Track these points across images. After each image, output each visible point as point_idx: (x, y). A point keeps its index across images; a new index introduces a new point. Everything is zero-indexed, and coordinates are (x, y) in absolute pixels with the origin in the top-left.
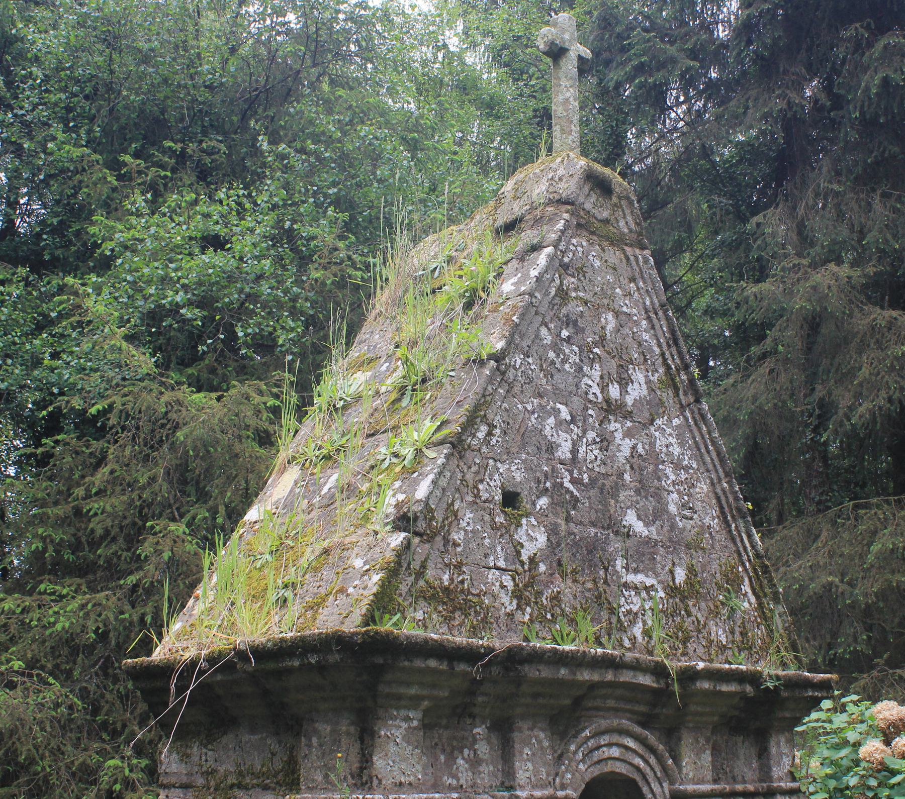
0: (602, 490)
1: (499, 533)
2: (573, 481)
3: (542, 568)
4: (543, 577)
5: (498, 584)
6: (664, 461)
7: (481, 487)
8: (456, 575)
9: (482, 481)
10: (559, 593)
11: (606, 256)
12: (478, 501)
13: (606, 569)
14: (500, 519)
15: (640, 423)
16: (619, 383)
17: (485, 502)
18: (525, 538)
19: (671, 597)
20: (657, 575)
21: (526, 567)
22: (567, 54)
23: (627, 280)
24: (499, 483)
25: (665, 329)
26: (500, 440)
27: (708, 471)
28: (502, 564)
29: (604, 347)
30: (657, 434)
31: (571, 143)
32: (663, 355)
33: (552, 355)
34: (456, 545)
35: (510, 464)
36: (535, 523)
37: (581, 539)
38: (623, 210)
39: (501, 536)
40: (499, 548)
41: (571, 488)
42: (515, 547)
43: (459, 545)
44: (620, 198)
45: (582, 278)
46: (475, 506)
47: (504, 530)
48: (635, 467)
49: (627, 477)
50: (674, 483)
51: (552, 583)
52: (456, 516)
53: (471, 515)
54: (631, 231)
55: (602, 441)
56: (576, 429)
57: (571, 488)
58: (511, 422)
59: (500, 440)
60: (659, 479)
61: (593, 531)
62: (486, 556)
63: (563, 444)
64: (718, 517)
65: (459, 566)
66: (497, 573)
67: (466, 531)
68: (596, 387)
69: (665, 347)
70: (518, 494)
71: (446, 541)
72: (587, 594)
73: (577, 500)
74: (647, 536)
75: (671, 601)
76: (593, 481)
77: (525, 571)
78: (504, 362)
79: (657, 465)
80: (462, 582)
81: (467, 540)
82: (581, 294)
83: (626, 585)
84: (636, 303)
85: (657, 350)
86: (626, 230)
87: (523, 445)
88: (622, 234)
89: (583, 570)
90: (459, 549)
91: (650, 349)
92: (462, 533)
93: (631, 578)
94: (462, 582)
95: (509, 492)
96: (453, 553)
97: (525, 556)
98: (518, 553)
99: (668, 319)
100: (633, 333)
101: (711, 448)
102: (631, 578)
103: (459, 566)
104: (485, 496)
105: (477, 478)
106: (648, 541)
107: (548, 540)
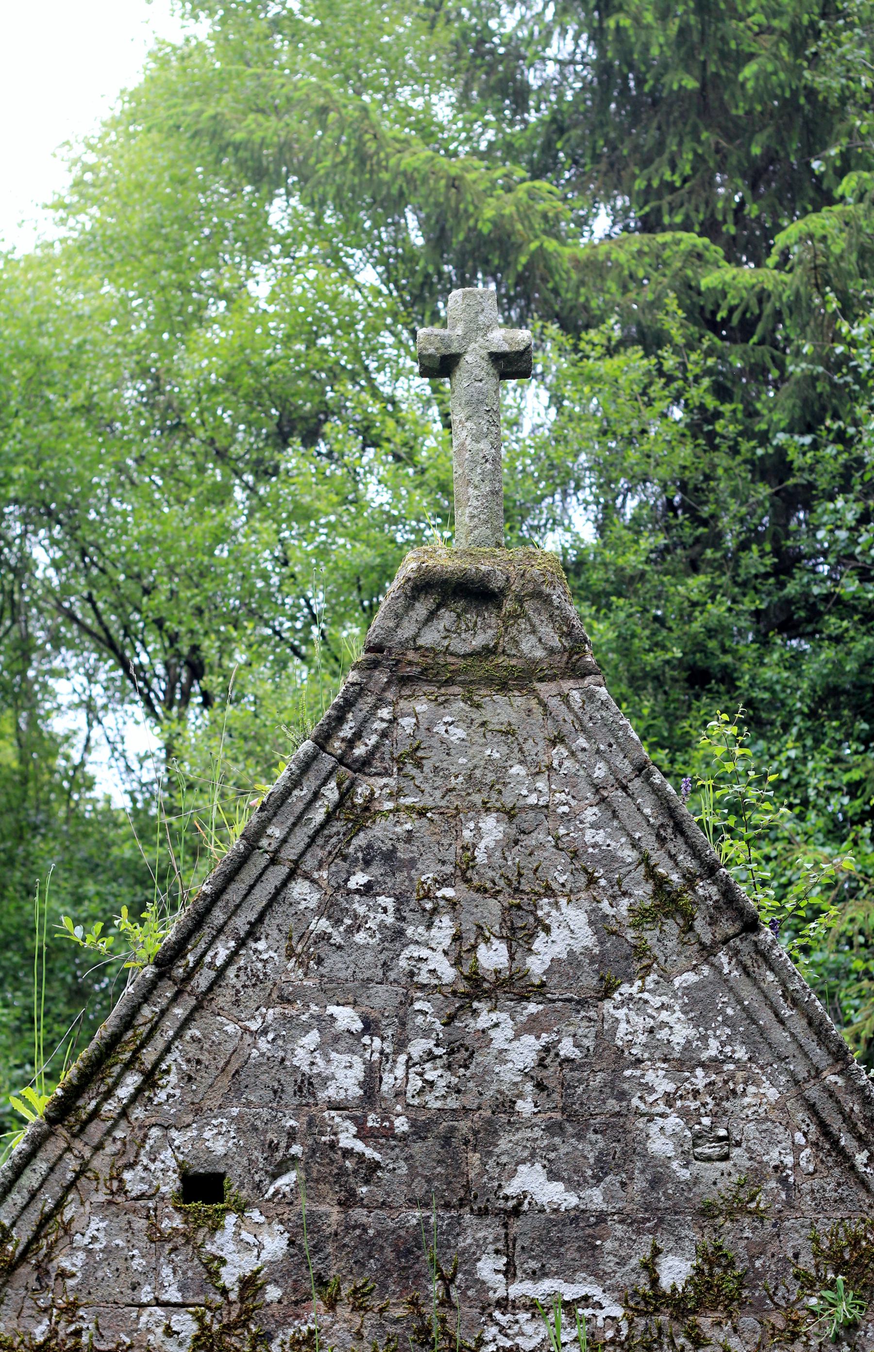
0: (446, 1140)
1: (168, 1246)
2: (362, 1134)
3: (273, 1293)
4: (275, 1309)
5: (160, 1330)
6: (639, 1061)
7: (127, 1175)
8: (63, 1324)
9: (131, 1166)
10: (311, 1333)
11: (487, 714)
12: (120, 1199)
13: (448, 1281)
14: (174, 1222)
15: (569, 1000)
16: (508, 940)
17: (137, 1198)
18: (231, 1247)
19: (641, 1313)
20: (599, 1277)
21: (233, 1296)
22: (462, 363)
23: (542, 744)
24: (173, 1164)
25: (647, 811)
26: (178, 1092)
27: (782, 1059)
28: (173, 1295)
29: (468, 881)
30: (621, 1013)
31: (467, 520)
32: (645, 860)
33: (323, 925)
34: (63, 1275)
35: (201, 1129)
36: (262, 1219)
37: (379, 1234)
38: (529, 620)
39: (174, 1249)
40: (166, 1271)
41: (359, 1146)
42: (205, 1265)
43: (73, 1275)
44: (520, 600)
45: (414, 772)
46: (114, 1208)
47: (180, 1240)
48: (551, 1083)
49: (525, 1107)
50: (669, 1099)
51: (298, 1316)
52: (66, 1232)
53: (102, 1225)
54: (552, 651)
55: (451, 1053)
56: (377, 1041)
57: (359, 1146)
58: (205, 1057)
59: (178, 1092)
60: (622, 1096)
61: (415, 1215)
62: (134, 1287)
63: (340, 1074)
64: (815, 1144)
65: (71, 1308)
66: (159, 1311)
67: (90, 1252)
68: (440, 956)
69: (649, 843)
70: (222, 1176)
71: (42, 1272)
72: (391, 1329)
73: (376, 1166)
74: (576, 1208)
75: (641, 1322)
76: (419, 1130)
77: (230, 1303)
78: (183, 962)
79: (616, 1073)
80: (78, 1333)
81: (90, 1268)
82: (409, 801)
83: (503, 1304)
84: (570, 780)
85: (629, 855)
86: (539, 653)
87: (237, 1089)
88: (535, 662)
89: (384, 1286)
90: (71, 1282)
91: (609, 858)
92: (81, 1255)
93: (520, 1289)
94: (78, 1333)
95: (198, 1176)
96: (59, 1290)
97: (229, 1277)
98: (215, 1275)
99: (657, 791)
100: (558, 838)
101: (786, 1012)
102: (520, 1289)
103: (71, 1308)
104: (136, 1189)
105: (120, 1163)
106: (577, 1216)
107: (291, 1243)
